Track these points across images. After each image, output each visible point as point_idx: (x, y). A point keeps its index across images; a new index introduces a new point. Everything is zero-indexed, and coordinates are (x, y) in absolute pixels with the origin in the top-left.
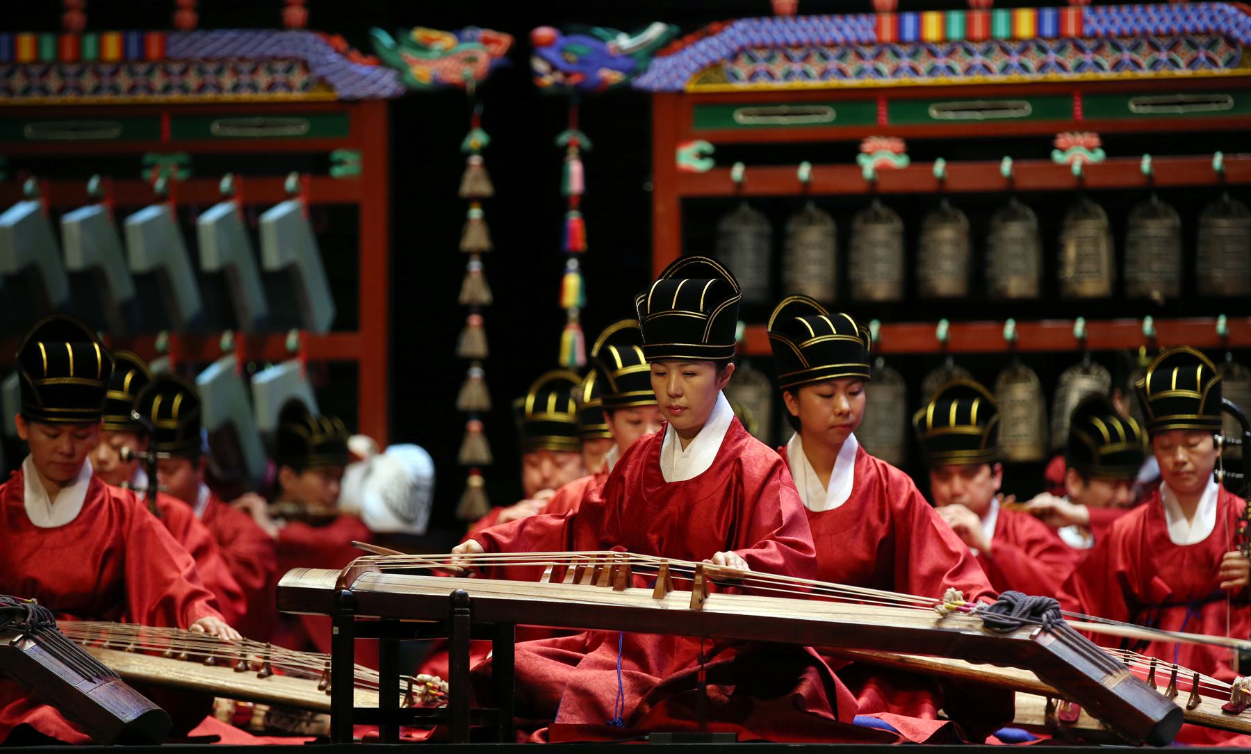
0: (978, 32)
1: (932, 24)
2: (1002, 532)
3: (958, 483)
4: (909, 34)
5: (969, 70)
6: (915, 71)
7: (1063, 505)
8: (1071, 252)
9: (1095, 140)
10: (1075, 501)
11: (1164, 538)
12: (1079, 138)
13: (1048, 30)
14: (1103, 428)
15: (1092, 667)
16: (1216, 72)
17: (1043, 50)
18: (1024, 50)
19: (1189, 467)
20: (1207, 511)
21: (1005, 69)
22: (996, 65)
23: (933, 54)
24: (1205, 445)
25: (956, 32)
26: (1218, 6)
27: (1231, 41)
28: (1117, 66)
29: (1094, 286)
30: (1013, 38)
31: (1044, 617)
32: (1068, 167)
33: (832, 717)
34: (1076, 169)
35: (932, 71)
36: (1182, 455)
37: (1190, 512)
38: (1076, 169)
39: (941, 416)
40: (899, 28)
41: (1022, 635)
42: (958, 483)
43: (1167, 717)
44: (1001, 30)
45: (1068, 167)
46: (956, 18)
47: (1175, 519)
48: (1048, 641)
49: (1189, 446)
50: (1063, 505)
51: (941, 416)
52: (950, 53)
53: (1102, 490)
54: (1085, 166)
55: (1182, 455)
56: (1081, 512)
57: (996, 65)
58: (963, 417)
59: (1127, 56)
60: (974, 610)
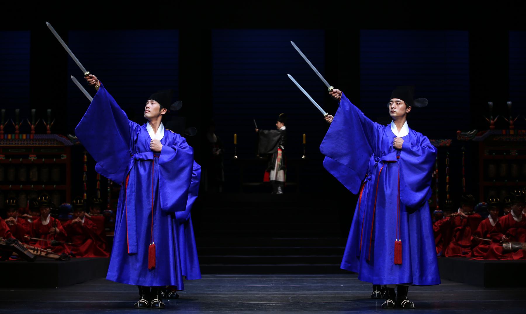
0: (17, 138)
1: (9, 136)
2: (18, 221)
3: (11, 213)
4: (6, 137)
5: (15, 144)
6: (7, 144)
7: (29, 216)
8: (31, 174)
9: (35, 156)
10: (30, 215)
11: (41, 224)
12: (33, 155)
13: (28, 138)
14: (35, 203)
15: (23, 250)
16: (54, 145)
17: (27, 141)
18: (24, 141)
19: (45, 213)
20: (48, 220)
21: (21, 144)
22: (20, 143)
23: (10, 141)
24: (48, 209)
25: (13, 137)
26: (55, 135)
27: (57, 141)
28: (39, 144)
29: (35, 179)
30: (22, 139)
31: (15, 242)
32: (31, 160)
33: (13, 224)
34: (32, 160)
35: (9, 144)
36: (44, 211)
37: (45, 220)
38: (32, 160)
39: (9, 202)
40: (4, 136)
41: (12, 245)
42: (11, 213)
43: (34, 258)
44: (21, 137)
45: (31, 160)
46: (13, 135)
47: (43, 221)
48: (16, 246)
49: (46, 209)
50: (29, 216)
51: (9, 202)
52: (12, 141)
53: (35, 213)
54: (33, 160)
55: (44, 211)
56: (31, 216)
57: (20, 143)
58: (13, 202)
59: (41, 142)
60: (4, 241)
